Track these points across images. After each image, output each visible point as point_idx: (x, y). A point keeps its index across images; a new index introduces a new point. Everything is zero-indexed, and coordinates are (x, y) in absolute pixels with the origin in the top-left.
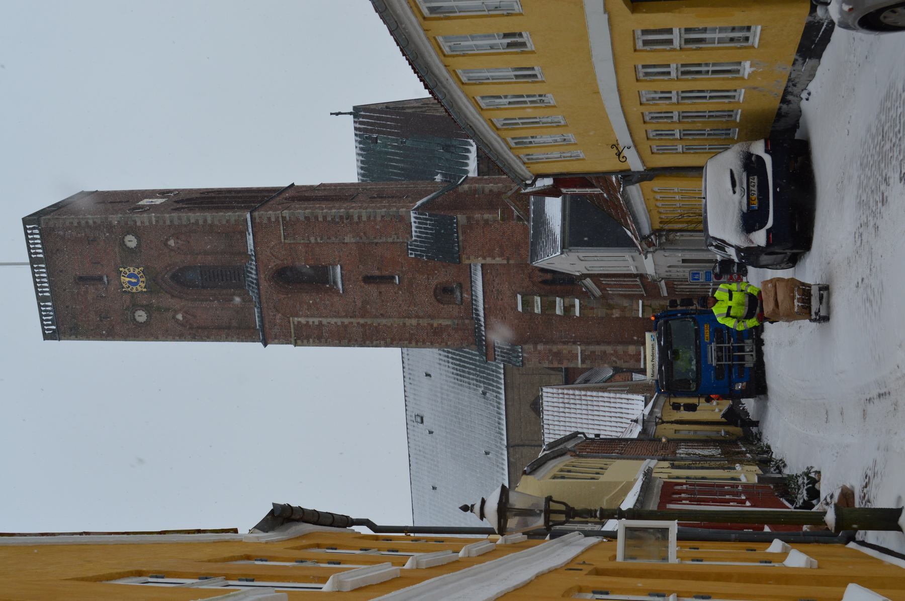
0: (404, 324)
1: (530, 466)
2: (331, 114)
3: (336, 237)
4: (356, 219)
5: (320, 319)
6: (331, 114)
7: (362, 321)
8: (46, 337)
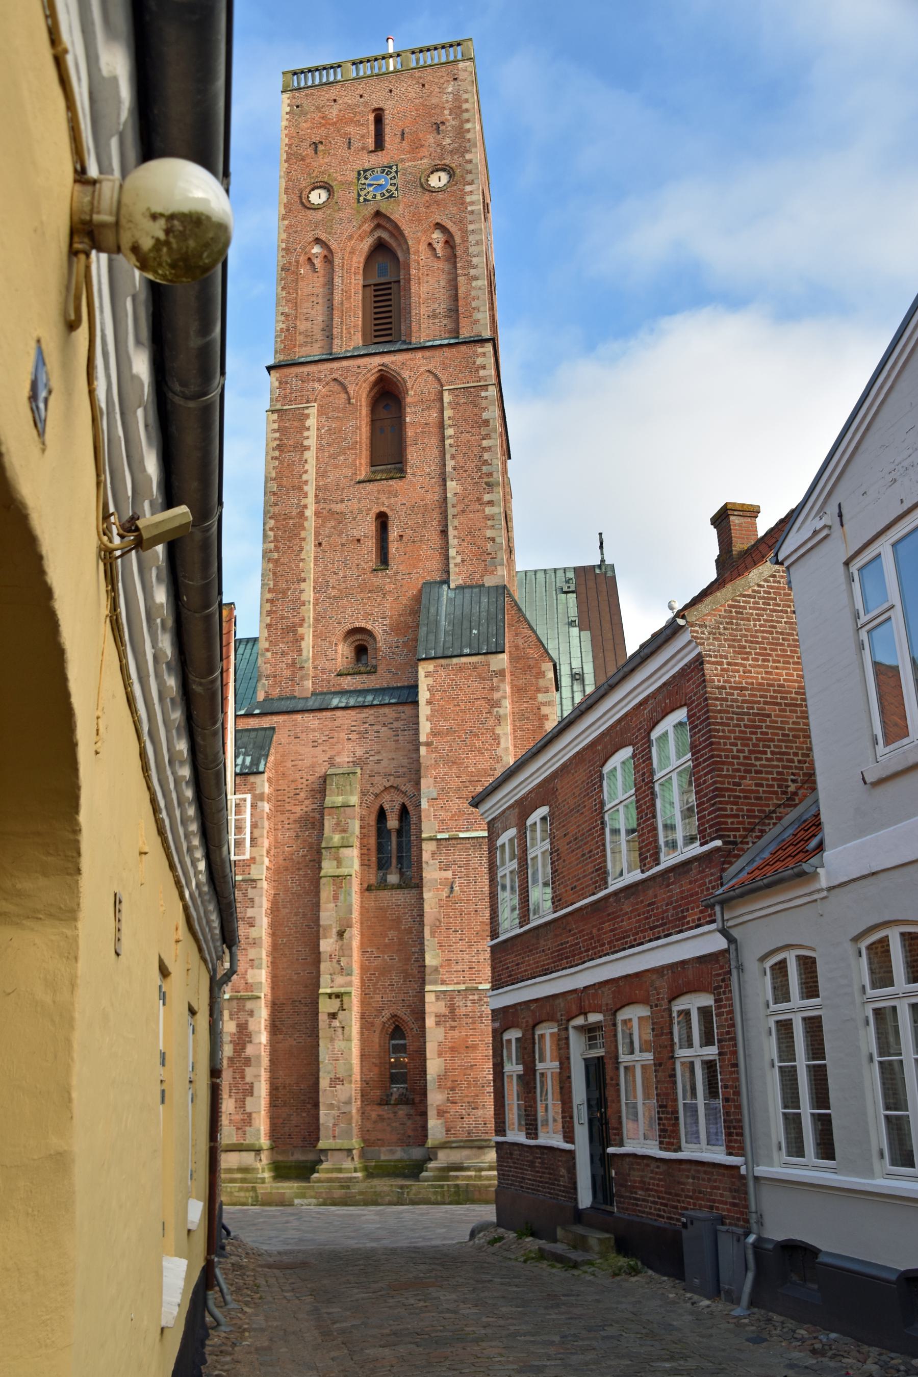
2: (600, 534)
3: (454, 468)
6: (600, 534)
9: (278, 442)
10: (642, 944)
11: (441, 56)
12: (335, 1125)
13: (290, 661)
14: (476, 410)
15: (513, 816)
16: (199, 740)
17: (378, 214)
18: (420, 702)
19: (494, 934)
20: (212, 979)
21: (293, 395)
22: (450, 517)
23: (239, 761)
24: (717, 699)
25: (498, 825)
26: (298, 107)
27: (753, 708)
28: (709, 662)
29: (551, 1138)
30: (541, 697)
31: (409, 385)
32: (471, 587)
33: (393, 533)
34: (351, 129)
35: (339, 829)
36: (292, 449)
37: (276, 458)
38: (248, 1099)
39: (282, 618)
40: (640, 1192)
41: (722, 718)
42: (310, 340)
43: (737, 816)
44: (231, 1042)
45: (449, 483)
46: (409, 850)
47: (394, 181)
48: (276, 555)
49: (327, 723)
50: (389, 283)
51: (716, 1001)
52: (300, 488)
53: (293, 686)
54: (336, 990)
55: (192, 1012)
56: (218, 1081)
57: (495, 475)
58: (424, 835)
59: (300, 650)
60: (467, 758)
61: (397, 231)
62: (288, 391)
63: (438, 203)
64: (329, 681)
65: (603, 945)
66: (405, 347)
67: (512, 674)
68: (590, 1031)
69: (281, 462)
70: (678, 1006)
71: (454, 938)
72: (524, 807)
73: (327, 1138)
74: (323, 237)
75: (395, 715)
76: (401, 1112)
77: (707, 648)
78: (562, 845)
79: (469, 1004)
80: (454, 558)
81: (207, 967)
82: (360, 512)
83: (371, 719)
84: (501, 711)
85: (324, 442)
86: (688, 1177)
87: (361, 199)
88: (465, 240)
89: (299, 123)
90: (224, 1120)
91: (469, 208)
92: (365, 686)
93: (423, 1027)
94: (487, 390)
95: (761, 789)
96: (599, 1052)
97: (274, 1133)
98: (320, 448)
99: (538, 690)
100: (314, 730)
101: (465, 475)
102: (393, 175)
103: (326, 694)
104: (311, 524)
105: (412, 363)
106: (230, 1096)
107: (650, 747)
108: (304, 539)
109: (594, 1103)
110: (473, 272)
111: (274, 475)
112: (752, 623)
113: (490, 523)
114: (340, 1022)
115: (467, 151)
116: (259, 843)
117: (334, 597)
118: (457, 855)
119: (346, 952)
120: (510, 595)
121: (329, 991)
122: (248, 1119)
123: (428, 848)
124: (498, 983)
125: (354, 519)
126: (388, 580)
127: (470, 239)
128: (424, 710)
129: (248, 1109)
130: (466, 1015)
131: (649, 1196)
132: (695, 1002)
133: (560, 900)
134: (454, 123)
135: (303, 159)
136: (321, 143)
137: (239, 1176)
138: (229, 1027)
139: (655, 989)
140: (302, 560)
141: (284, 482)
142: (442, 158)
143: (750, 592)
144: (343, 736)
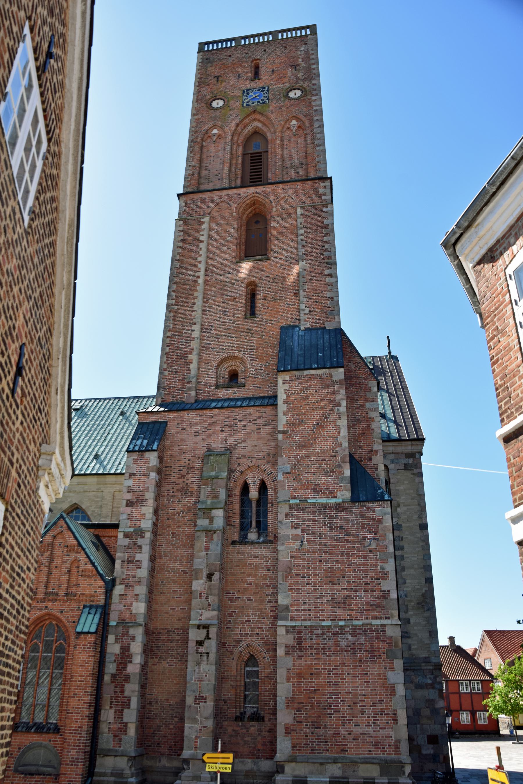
0: (195, 324)
2: (388, 337)
3: (304, 253)
5: (205, 242)
6: (388, 337)
7: (201, 281)
8: (202, 45)
9: (182, 238)
14: (319, 219)
21: (194, 211)
32: (317, 329)
34: (240, 70)
36: (192, 242)
37: (180, 247)
38: (126, 711)
39: (178, 349)
42: (207, 181)
44: (115, 661)
46: (266, 516)
48: (176, 308)
49: (206, 419)
50: (261, 153)
52: (196, 266)
53: (182, 394)
54: (204, 622)
62: (191, 208)
64: (209, 392)
71: (303, 582)
75: (257, 414)
79: (314, 637)
80: (303, 310)
83: (240, 417)
89: (207, 67)
91: (314, 108)
92: (236, 396)
93: (275, 657)
94: (327, 207)
99: (367, 400)
100: (196, 424)
101: (312, 257)
102: (265, 92)
105: (276, 192)
106: (111, 707)
108: (196, 298)
111: (178, 258)
115: (313, 79)
118: (306, 517)
121: (197, 622)
125: (233, 285)
126: (255, 325)
128: (282, 407)
129: (125, 720)
130: (311, 647)
136: (221, 76)
141: (185, 262)
142: (297, 82)
144: (218, 428)
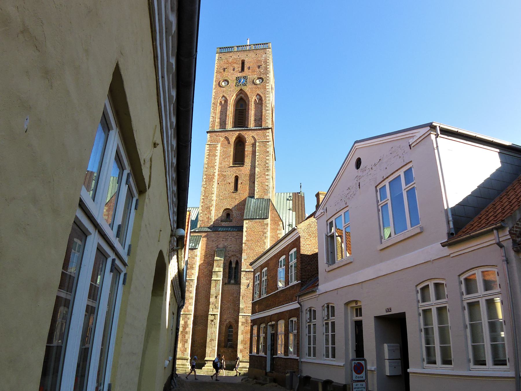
1: (94, 173)
3: (258, 164)
4: (267, 173)
7: (216, 174)
9: (208, 153)
10: (284, 305)
11: (262, 47)
12: (210, 353)
13: (207, 217)
15: (259, 270)
16: (179, 263)
17: (241, 90)
18: (244, 231)
19: (253, 300)
20: (178, 307)
22: (256, 178)
23: (191, 245)
24: (303, 247)
25: (256, 271)
26: (220, 58)
27: (311, 249)
28: (302, 238)
29: (262, 354)
30: (278, 232)
31: (247, 139)
33: (239, 182)
35: (218, 266)
38: (186, 344)
40: (280, 367)
41: (303, 251)
43: (305, 275)
45: (256, 169)
47: (246, 81)
50: (243, 109)
51: (297, 320)
52: (214, 167)
55: (173, 314)
56: (178, 331)
57: (269, 167)
58: (242, 270)
59: (210, 214)
60: (256, 248)
61: (246, 95)
63: (258, 88)
64: (218, 223)
65: (276, 304)
66: (246, 129)
67: (271, 225)
68: (272, 326)
69: (209, 159)
70: (291, 319)
72: (262, 267)
73: (208, 357)
74: (225, 95)
76: (230, 350)
77: (302, 234)
78: (269, 278)
80: (256, 190)
81: (177, 304)
82: (231, 175)
84: (266, 235)
85: (222, 154)
86: (289, 362)
87: (237, 85)
88: (265, 99)
90: (178, 350)
91: (267, 90)
95: (312, 269)
96: (273, 332)
97: (192, 355)
98: (221, 156)
100: (213, 237)
102: (246, 79)
103: (217, 227)
104: (216, 177)
107: (289, 256)
109: (272, 345)
110: (267, 108)
112: (313, 229)
113: (267, 181)
114: (214, 323)
116: (195, 269)
117: (221, 199)
119: (217, 302)
120: (271, 202)
121: (212, 313)
122: (185, 350)
123: (243, 274)
124: (253, 312)
125: (229, 177)
126: (237, 195)
127: (267, 99)
128: (245, 234)
131: (281, 367)
132: (295, 319)
133: (268, 292)
134: (264, 65)
135: (221, 73)
137: (182, 366)
138: (182, 322)
139: (286, 316)
140: (213, 188)
143: (313, 221)
